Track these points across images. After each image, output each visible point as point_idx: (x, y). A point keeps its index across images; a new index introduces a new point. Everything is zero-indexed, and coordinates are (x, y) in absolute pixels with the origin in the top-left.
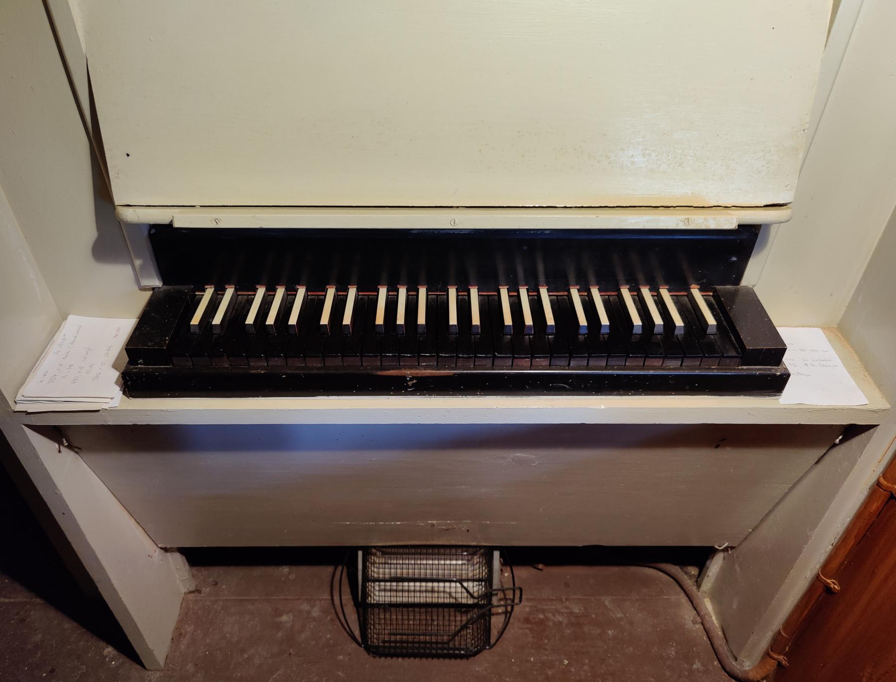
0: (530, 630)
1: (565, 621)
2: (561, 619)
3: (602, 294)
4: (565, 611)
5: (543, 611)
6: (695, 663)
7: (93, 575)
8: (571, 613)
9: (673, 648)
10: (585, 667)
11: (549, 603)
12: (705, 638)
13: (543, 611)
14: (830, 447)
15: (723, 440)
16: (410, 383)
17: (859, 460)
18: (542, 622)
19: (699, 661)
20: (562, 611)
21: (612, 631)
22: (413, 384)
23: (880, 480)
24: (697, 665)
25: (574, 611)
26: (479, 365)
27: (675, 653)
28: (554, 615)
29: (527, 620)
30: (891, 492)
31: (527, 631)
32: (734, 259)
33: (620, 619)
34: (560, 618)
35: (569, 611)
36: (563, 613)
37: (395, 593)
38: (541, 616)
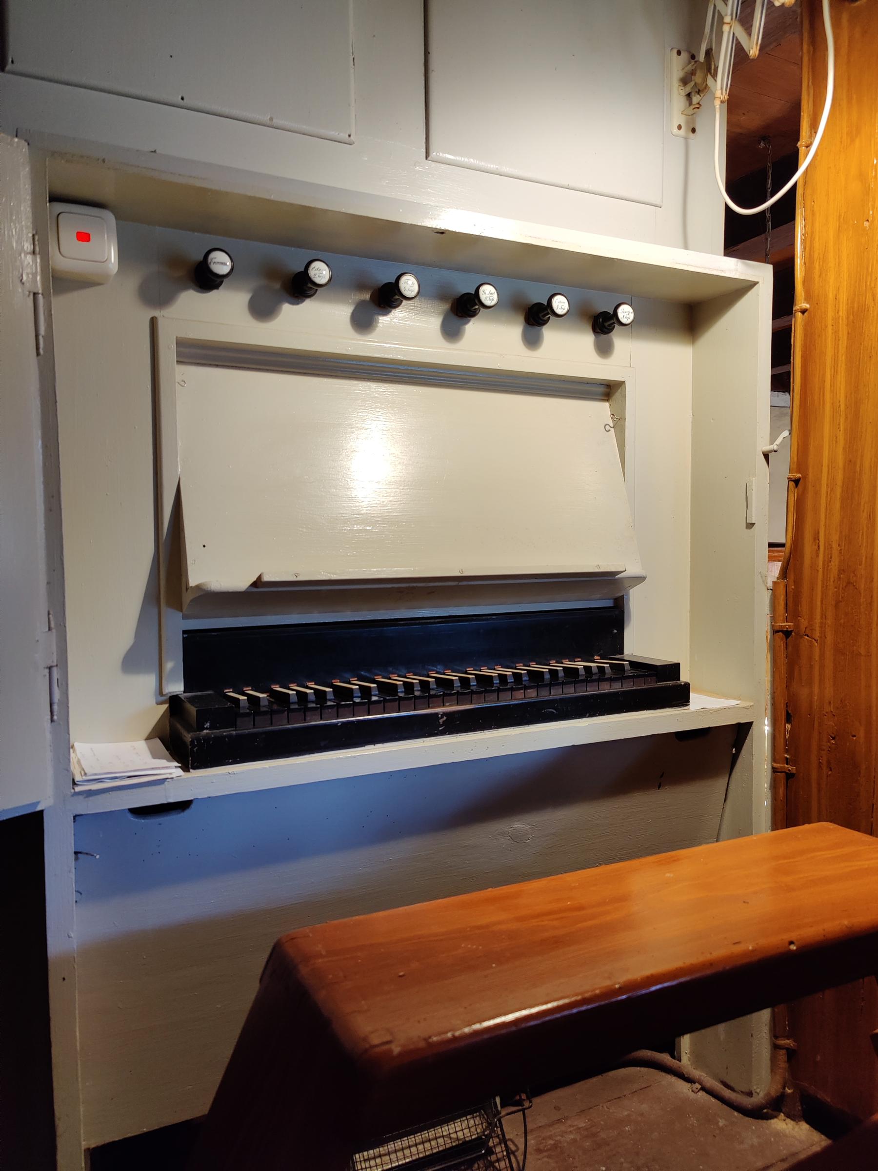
0: (549, 1157)
1: (578, 1137)
2: (573, 1137)
3: (769, 210)
4: (572, 1129)
5: (550, 1137)
6: (719, 1121)
7: (59, 1119)
8: (579, 1128)
9: (692, 1119)
10: (625, 1165)
11: (551, 1129)
12: (713, 1100)
13: (550, 1137)
14: (729, 773)
15: (662, 776)
16: (441, 721)
17: (754, 762)
18: (555, 1146)
19: (721, 1119)
20: (569, 1130)
21: (629, 1127)
22: (443, 722)
23: (774, 766)
24: (721, 1123)
25: (580, 1126)
26: (488, 700)
27: (696, 1121)
28: (562, 1136)
29: (539, 1151)
30: (785, 772)
31: (546, 1159)
32: (615, 631)
33: (628, 1115)
34: (572, 1136)
35: (575, 1128)
36: (570, 1131)
37: (387, 1157)
38: (551, 1142)
